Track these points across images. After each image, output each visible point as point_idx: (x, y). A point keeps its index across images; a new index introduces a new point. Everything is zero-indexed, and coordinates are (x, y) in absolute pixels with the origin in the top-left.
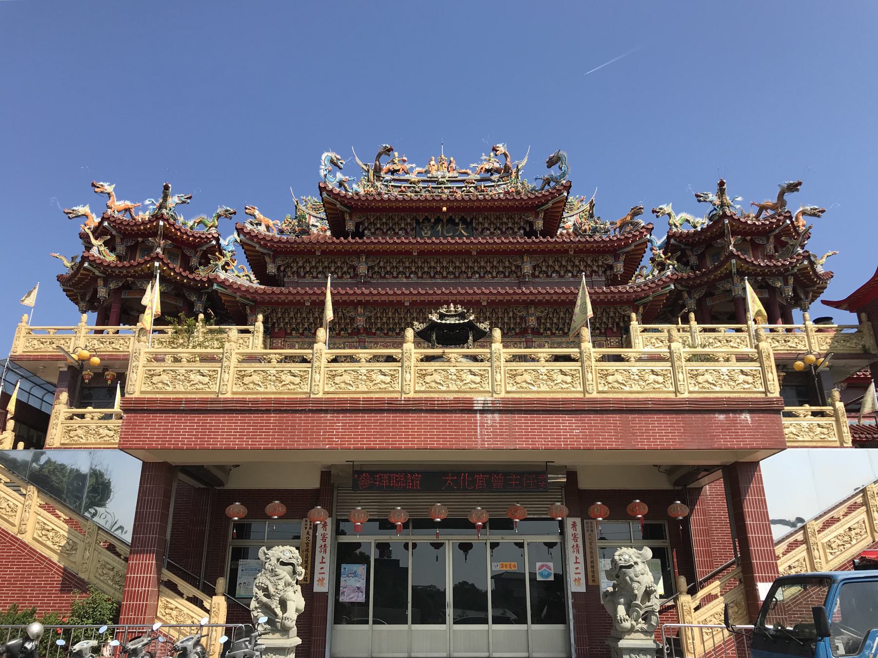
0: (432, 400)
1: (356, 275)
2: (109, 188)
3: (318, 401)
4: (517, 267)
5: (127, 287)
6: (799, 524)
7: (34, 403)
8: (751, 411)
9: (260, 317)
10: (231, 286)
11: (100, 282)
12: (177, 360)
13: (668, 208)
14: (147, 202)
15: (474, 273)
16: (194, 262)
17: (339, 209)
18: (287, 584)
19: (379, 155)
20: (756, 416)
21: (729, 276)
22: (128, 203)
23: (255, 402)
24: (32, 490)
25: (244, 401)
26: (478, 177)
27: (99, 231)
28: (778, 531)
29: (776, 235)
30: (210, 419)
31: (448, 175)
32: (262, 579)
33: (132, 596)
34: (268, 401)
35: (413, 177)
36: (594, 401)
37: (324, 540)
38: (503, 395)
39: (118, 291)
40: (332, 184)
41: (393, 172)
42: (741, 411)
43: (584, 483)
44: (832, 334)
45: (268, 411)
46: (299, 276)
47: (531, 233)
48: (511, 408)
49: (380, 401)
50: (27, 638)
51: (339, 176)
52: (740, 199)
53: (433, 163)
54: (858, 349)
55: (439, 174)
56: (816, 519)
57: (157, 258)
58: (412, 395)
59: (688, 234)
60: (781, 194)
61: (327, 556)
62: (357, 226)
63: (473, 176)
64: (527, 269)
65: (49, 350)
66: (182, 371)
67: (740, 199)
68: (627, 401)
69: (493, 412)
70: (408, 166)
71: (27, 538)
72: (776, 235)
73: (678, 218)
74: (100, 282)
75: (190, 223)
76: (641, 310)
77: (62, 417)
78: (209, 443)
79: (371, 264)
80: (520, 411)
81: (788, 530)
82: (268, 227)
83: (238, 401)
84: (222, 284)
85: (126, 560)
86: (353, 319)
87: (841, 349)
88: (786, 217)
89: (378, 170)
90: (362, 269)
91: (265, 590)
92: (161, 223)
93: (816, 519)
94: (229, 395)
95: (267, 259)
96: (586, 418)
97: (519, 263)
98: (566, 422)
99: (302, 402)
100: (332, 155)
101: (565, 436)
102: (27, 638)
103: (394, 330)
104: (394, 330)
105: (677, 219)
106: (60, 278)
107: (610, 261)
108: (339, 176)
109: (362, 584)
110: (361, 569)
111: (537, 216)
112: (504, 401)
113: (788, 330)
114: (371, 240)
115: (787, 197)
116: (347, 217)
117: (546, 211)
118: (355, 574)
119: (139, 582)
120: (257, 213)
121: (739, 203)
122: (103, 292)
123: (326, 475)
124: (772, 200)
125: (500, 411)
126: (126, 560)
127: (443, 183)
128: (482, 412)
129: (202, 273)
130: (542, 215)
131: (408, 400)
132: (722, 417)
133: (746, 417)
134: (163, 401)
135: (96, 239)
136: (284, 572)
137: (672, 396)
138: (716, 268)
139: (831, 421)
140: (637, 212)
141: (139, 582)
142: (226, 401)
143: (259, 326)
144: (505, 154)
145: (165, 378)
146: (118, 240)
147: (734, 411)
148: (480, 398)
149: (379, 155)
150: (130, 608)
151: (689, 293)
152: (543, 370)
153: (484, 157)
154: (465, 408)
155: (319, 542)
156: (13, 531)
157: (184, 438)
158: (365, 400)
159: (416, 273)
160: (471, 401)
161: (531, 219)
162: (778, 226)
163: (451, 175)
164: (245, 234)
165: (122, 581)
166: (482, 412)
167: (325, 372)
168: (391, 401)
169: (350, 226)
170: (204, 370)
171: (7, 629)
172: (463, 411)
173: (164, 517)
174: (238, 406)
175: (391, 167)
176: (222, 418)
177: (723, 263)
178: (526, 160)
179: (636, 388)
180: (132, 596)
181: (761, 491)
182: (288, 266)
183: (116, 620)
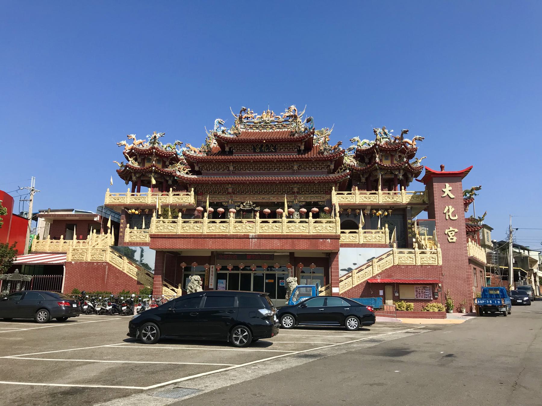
0: (237, 235)
1: (229, 170)
2: (133, 136)
3: (205, 235)
4: (292, 166)
5: (143, 175)
6: (350, 270)
7: (116, 220)
8: (330, 239)
9: (193, 189)
10: (181, 178)
11: (133, 175)
12: (164, 222)
13: (357, 138)
14: (147, 136)
15: (275, 169)
16: (167, 163)
17: (221, 141)
18: (197, 286)
19: (241, 111)
20: (332, 240)
21: (376, 169)
22: (141, 141)
23: (187, 235)
24: (125, 258)
25: (184, 235)
26: (283, 120)
27: (131, 154)
28: (342, 273)
29: (399, 151)
30: (175, 240)
31: (270, 119)
32: (190, 284)
33: (156, 288)
34: (191, 235)
35: (256, 120)
36: (284, 235)
37: (212, 272)
38: (258, 233)
39: (139, 177)
40: (219, 133)
41: (248, 118)
42: (328, 239)
43: (296, 255)
44: (412, 195)
45: (191, 238)
46: (207, 170)
47: (299, 152)
48: (260, 237)
49: (223, 235)
50: (132, 298)
51: (223, 128)
52: (392, 131)
53: (264, 114)
54: (421, 201)
55: (267, 119)
56: (356, 269)
57: (154, 166)
58: (232, 233)
59: (367, 150)
60: (402, 134)
61: (213, 277)
62: (230, 148)
63: (282, 120)
64: (296, 167)
65: (117, 202)
66: (166, 226)
67: (392, 131)
68: (294, 235)
69: (255, 238)
70: (253, 115)
71: (125, 272)
72: (399, 151)
73: (361, 142)
74: (133, 175)
75: (165, 146)
76: (338, 185)
77: (128, 232)
78: (175, 247)
79: (234, 166)
80: (263, 238)
81: (347, 272)
82: (195, 151)
83: (182, 235)
84: (178, 177)
85: (153, 278)
86: (227, 189)
87: (414, 202)
88: (402, 145)
89: (241, 118)
90: (231, 168)
91: (191, 287)
92: (154, 168)
93: (356, 269)
94: (180, 233)
95: (195, 165)
96: (282, 240)
97: (292, 165)
98: (276, 241)
99: (200, 235)
100: (219, 120)
101: (276, 245)
102: (132, 298)
103: (243, 192)
104: (243, 192)
105: (361, 143)
106: (117, 171)
107: (329, 164)
108: (223, 128)
109: (224, 286)
110: (224, 281)
111: (302, 144)
112: (258, 235)
113: (395, 194)
114: (234, 157)
115: (404, 135)
116: (226, 145)
117: (305, 142)
118: (222, 283)
119: (157, 284)
120: (190, 146)
121: (391, 133)
122: (135, 178)
123: (212, 252)
124: (398, 136)
125: (257, 238)
126: (153, 278)
127: (268, 123)
128: (252, 238)
129: (170, 169)
130: (303, 144)
131: (230, 235)
132: (321, 240)
133: (329, 240)
134: (161, 235)
135: (130, 157)
136: (196, 283)
137: (308, 234)
138: (370, 167)
139: (383, 235)
140: (339, 144)
141: (157, 284)
142: (179, 235)
143: (192, 193)
144: (295, 110)
145: (161, 228)
146: (138, 156)
147: (325, 239)
148: (251, 234)
149: (241, 111)
150: (155, 291)
151: (363, 175)
152: (270, 226)
153: (286, 110)
154: (246, 237)
155: (211, 273)
156: (121, 269)
157: (167, 245)
158: (218, 235)
159: (252, 169)
160: (248, 235)
161: (299, 145)
162: (399, 148)
163: (272, 119)
164: (186, 156)
165: (152, 284)
166: (252, 238)
167: (206, 227)
168: (225, 235)
169: (227, 149)
170: (172, 226)
171: (514, 252)
172: (246, 238)
173: (163, 266)
174: (182, 236)
175: (246, 115)
176: (178, 240)
177: (373, 165)
178: (304, 111)
179: (297, 231)
180: (156, 288)
181: (338, 261)
182: (203, 166)
183: (152, 294)
